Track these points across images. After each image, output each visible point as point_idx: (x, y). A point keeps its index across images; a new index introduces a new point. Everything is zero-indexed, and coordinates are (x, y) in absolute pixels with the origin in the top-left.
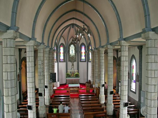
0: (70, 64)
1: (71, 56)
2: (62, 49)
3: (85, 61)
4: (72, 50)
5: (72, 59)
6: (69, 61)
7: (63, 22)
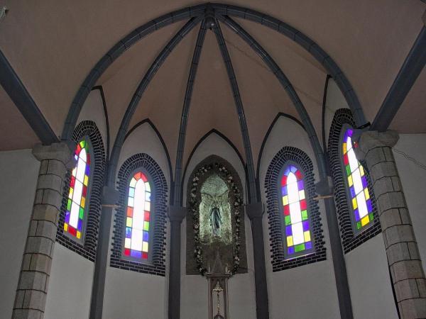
0: (194, 287)
1: (212, 242)
2: (137, 242)
3: (319, 256)
4: (216, 211)
5: (211, 262)
6: (188, 273)
7: (249, 127)
